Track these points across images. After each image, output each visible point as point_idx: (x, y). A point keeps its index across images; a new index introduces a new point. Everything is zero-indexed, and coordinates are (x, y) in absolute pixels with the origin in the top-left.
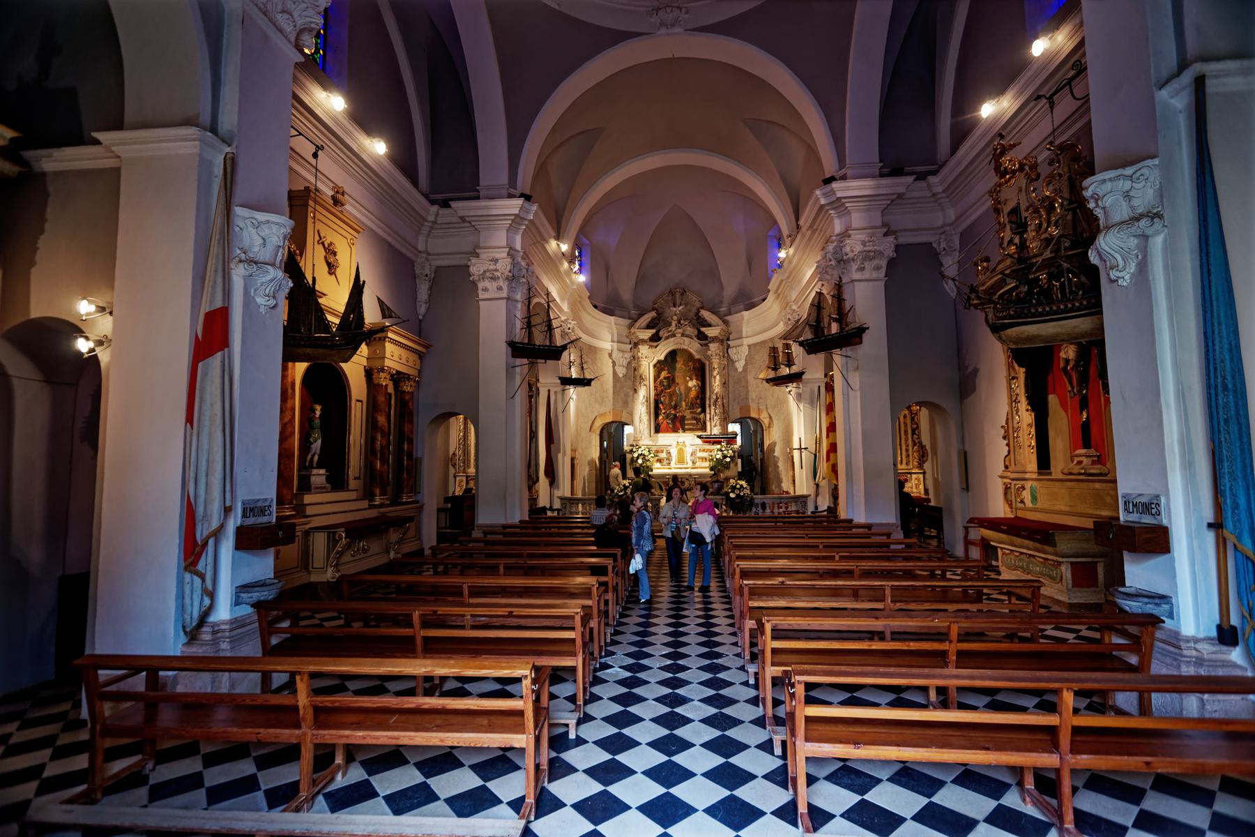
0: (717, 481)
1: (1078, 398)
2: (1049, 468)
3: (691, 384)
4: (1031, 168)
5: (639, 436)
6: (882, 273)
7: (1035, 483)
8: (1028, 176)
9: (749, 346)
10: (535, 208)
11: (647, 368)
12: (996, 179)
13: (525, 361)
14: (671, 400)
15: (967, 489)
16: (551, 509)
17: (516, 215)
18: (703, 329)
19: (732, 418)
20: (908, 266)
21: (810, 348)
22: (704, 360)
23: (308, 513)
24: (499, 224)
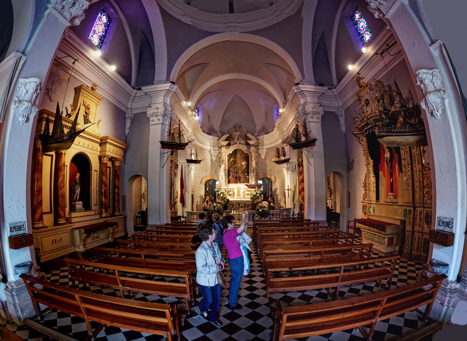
0: (254, 204)
1: (390, 173)
3: (243, 163)
5: (221, 184)
6: (320, 120)
7: (375, 205)
10: (176, 86)
11: (225, 157)
13: (168, 150)
16: (183, 217)
17: (168, 90)
19: (260, 178)
20: (328, 119)
21: (294, 146)
22: (248, 154)
23: (73, 221)
24: (161, 94)
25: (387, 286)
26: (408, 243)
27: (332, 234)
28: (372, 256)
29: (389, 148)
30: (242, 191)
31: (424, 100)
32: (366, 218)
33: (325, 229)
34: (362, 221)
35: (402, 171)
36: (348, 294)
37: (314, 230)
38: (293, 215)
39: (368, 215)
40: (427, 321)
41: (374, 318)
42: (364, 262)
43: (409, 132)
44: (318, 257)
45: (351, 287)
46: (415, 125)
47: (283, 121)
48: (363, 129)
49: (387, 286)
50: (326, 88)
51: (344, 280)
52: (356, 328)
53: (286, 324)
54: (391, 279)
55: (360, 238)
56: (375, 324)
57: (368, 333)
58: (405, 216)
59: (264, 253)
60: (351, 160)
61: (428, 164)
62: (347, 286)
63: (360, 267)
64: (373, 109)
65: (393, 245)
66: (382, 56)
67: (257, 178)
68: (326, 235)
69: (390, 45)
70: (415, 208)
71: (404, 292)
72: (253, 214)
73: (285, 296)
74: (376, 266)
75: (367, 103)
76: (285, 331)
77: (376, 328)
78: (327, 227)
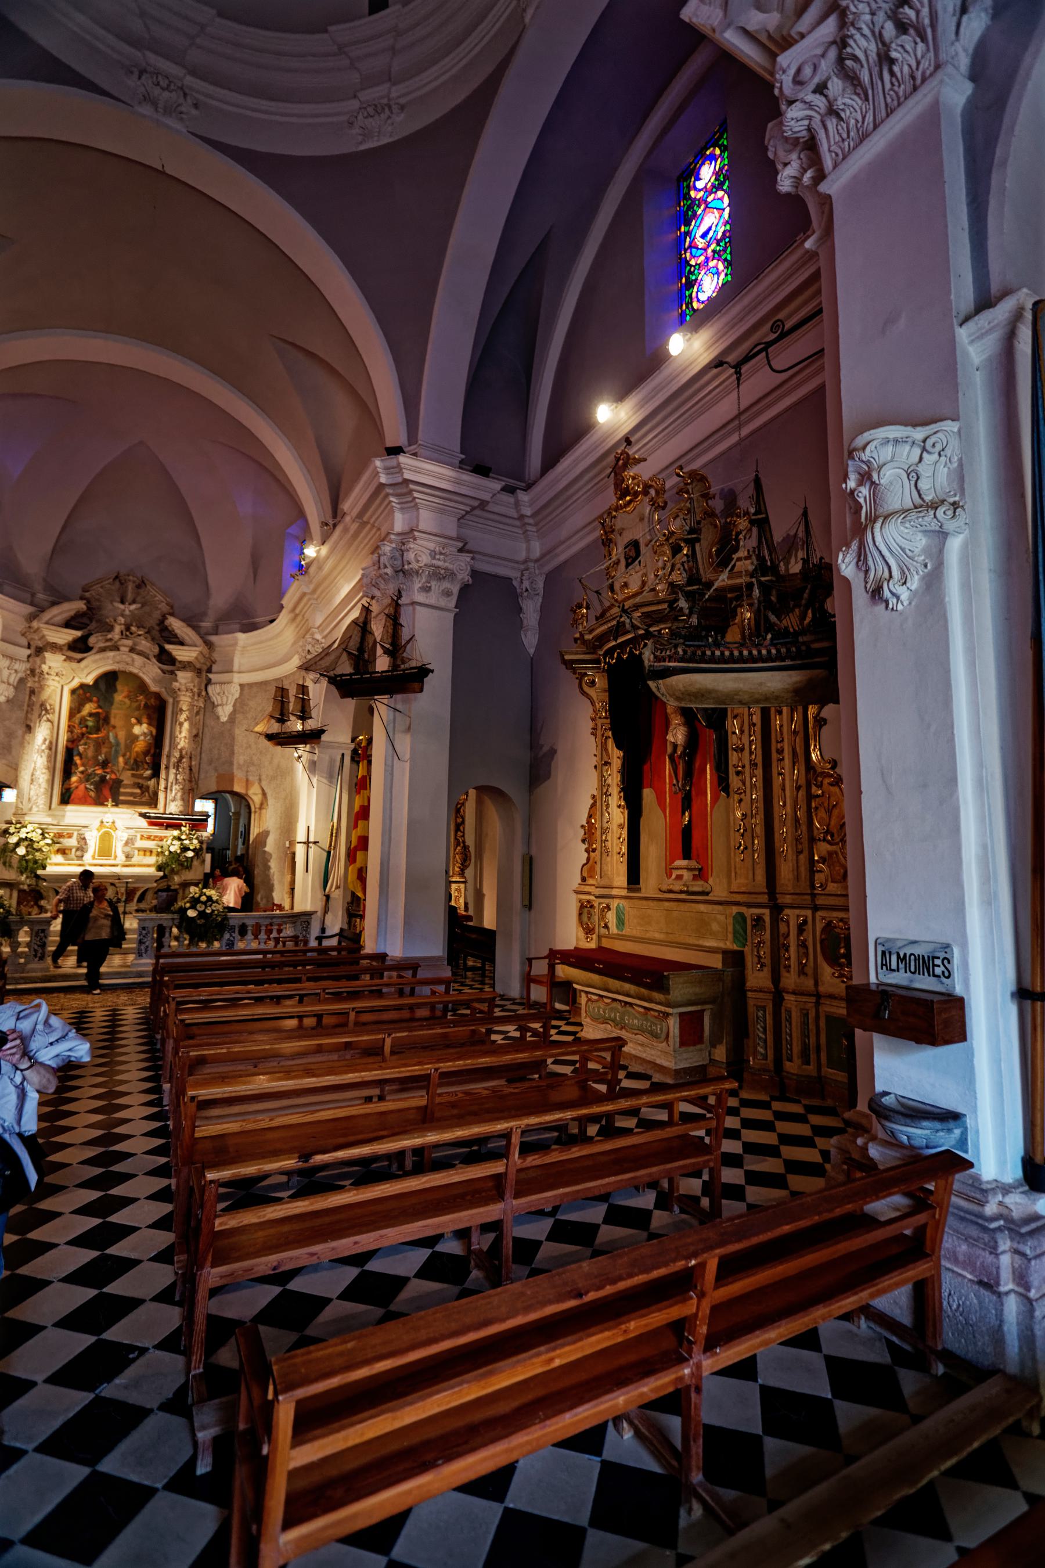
0: (168, 889)
1: (680, 796)
2: (638, 883)
3: (137, 730)
4: (657, 492)
5: (25, 807)
6: (452, 602)
7: (623, 903)
8: (653, 502)
9: (242, 686)
12: (613, 500)
14: (98, 751)
15: (530, 907)
18: (168, 647)
19: (203, 790)
20: (483, 600)
21: (344, 687)
25: (705, 1202)
26: (761, 1030)
27: (467, 1004)
28: (626, 1083)
29: (688, 716)
30: (120, 837)
31: (854, 546)
32: (593, 945)
33: (441, 988)
34: (578, 958)
35: (726, 789)
36: (549, 1250)
37: (401, 993)
38: (319, 939)
39: (600, 937)
40: (941, 1370)
41: (682, 1360)
42: (596, 1109)
43: (769, 658)
44: (417, 1099)
45: (560, 1216)
46: (796, 634)
47: (314, 591)
48: (600, 647)
49: (705, 1202)
50: (497, 486)
51: (526, 1185)
52: (617, 1420)
53: (293, 1457)
54: (714, 1174)
55: (571, 1016)
56: (698, 1390)
57: (678, 1444)
58: (740, 935)
59: (193, 1098)
60: (545, 749)
61: (834, 764)
62: (541, 1213)
63: (583, 1130)
64: (648, 579)
65: (700, 1040)
66: (738, 373)
67: (191, 790)
68: (445, 1010)
69: (788, 325)
70: (777, 909)
71: (787, 1228)
72: (161, 930)
73: (286, 1293)
74: (647, 1125)
75: (633, 554)
76: (291, 1500)
77: (708, 1415)
78: (447, 982)
